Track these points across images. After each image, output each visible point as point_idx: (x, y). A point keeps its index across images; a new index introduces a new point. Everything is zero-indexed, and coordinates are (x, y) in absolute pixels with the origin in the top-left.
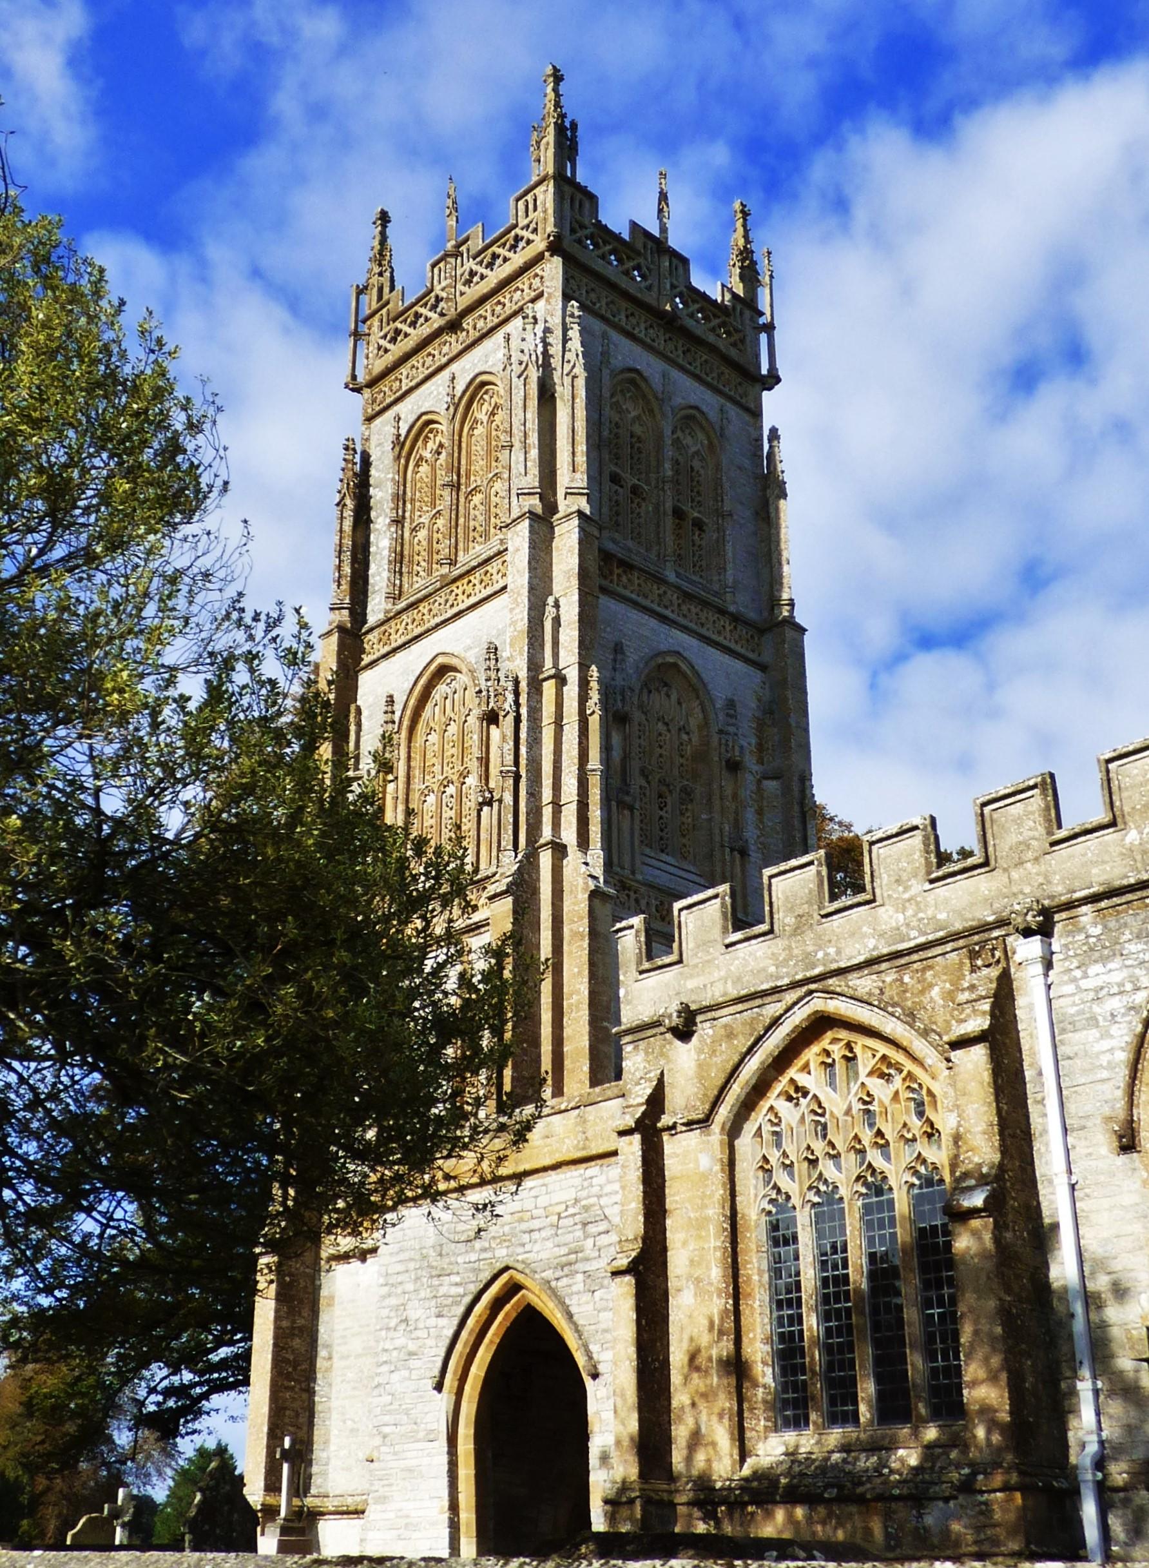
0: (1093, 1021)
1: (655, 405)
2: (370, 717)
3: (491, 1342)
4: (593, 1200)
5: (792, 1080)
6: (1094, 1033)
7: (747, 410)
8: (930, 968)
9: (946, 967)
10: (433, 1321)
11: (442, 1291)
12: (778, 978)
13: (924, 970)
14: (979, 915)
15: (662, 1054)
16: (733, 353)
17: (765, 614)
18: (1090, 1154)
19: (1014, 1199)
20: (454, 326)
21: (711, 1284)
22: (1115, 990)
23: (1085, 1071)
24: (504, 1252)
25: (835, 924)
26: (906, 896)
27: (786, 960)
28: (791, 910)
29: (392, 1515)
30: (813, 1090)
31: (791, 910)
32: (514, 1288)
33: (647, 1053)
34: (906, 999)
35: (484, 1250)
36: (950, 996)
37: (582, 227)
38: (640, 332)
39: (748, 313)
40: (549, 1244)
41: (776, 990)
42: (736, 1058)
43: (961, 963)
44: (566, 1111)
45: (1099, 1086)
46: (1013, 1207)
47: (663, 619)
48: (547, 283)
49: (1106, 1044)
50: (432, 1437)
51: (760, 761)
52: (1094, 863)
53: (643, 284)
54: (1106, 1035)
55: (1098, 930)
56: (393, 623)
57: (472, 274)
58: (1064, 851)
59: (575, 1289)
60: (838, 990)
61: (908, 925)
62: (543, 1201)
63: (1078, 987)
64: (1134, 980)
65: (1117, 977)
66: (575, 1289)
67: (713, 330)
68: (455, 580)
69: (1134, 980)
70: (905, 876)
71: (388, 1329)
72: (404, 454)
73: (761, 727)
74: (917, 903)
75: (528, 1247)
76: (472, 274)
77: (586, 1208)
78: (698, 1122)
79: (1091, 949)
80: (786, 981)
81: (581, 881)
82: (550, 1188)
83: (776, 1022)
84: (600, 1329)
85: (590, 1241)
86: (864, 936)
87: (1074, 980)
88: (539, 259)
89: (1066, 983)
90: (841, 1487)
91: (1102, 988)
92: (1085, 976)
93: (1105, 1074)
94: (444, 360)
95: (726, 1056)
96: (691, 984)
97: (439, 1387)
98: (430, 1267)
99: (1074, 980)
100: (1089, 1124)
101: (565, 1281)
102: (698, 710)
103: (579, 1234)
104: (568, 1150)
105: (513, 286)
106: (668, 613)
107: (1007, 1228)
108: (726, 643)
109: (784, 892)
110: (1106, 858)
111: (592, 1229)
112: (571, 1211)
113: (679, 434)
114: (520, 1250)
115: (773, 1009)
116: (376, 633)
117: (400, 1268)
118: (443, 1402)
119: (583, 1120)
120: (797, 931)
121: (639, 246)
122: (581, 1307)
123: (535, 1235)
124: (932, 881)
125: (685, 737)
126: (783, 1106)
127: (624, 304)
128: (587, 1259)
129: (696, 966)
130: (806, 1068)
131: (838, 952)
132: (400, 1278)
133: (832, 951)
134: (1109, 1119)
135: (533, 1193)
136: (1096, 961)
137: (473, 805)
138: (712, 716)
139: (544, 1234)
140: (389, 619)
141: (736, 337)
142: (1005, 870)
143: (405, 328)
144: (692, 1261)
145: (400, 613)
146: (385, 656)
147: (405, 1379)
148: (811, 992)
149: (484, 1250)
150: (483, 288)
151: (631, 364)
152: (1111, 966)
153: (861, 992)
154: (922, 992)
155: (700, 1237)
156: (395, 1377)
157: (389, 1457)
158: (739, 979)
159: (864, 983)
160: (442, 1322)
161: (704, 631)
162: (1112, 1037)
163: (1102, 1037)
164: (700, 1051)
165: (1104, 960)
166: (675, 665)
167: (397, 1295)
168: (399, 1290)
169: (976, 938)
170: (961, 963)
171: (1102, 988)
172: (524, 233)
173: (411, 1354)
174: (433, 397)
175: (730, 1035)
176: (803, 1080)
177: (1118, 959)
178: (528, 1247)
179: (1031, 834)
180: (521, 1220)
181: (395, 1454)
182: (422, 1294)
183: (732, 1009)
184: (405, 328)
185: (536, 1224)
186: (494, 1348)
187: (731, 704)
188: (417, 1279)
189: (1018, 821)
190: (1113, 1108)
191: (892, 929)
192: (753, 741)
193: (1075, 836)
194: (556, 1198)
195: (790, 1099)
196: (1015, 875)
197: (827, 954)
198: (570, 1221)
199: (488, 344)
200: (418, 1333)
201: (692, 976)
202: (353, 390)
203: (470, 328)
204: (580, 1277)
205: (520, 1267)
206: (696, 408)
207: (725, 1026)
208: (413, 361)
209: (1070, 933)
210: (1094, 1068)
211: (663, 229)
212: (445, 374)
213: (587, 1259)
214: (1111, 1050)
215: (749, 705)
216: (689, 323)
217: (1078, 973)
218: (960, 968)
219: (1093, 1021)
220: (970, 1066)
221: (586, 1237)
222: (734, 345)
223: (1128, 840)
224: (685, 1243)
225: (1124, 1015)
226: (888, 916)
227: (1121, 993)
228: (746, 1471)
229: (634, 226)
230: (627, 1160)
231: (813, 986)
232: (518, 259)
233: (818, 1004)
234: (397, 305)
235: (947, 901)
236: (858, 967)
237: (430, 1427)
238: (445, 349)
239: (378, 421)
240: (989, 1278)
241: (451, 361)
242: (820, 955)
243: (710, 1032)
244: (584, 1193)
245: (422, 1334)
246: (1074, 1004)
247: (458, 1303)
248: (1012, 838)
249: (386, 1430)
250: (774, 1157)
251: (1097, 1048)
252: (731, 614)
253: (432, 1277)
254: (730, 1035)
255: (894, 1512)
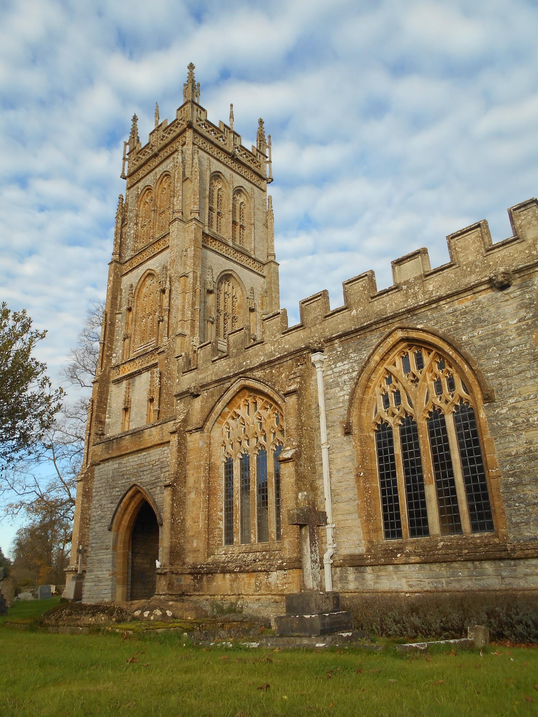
0: (338, 385)
1: (227, 184)
2: (125, 292)
3: (130, 512)
4: (165, 459)
5: (235, 412)
6: (338, 389)
7: (261, 189)
8: (282, 367)
9: (287, 366)
10: (110, 505)
11: (114, 493)
12: (230, 373)
13: (280, 368)
14: (299, 345)
15: (189, 403)
16: (256, 170)
17: (265, 259)
18: (335, 436)
19: (305, 455)
20: (156, 155)
21: (201, 490)
22: (346, 372)
23: (334, 405)
24: (134, 479)
25: (250, 352)
26: (275, 339)
27: (233, 366)
28: (236, 347)
29: (93, 577)
30: (242, 415)
31: (236, 347)
32: (138, 492)
33: (184, 403)
34: (273, 379)
35: (127, 478)
36: (287, 377)
37: (201, 120)
38: (222, 159)
39: (262, 156)
40: (149, 476)
41: (229, 378)
42: (214, 403)
43: (293, 364)
44: (157, 425)
45: (339, 410)
46: (305, 458)
47: (227, 258)
48: (187, 139)
49: (342, 393)
50: (107, 548)
51: (262, 309)
52: (340, 324)
53: (223, 143)
54: (342, 390)
55: (340, 349)
56: (133, 259)
57: (163, 136)
58: (330, 319)
59: (157, 492)
60: (249, 376)
61: (275, 351)
62: (148, 460)
63: (333, 371)
64: (352, 367)
65: (347, 367)
66: (157, 492)
67: (241, 155)
68: (154, 243)
69: (352, 367)
70: (275, 332)
71: (95, 508)
72: (139, 200)
73: (263, 297)
74: (279, 342)
75: (142, 477)
76: (163, 136)
77: (162, 462)
78: (199, 428)
79: (338, 356)
80: (232, 374)
81: (191, 348)
82: (151, 455)
83: (228, 389)
84: (163, 500)
85: (163, 474)
86: (260, 355)
87: (332, 369)
88: (184, 131)
89: (329, 370)
90: (241, 567)
91: (341, 371)
92: (336, 367)
93: (341, 405)
94: (153, 167)
95: (211, 402)
96: (200, 377)
97: (110, 529)
98: (110, 485)
99: (332, 369)
100: (335, 424)
101: (154, 489)
102: (240, 290)
103: (159, 472)
104: (157, 441)
105: (177, 140)
106: (229, 256)
107: (301, 465)
108: (251, 268)
109: (233, 340)
110: (344, 321)
111: (164, 470)
112: (157, 463)
113: (236, 196)
114: (140, 478)
115: (227, 385)
116: (128, 263)
117: (100, 485)
118: (111, 536)
119: (162, 429)
120: (237, 355)
121: (222, 129)
122: (158, 498)
123: (145, 473)
124: (283, 334)
125: (235, 300)
126: (230, 421)
127: (216, 149)
128: (161, 481)
129: (202, 369)
130: (239, 407)
131: (251, 362)
132: (101, 489)
133: (248, 362)
134: (342, 422)
135: (145, 457)
136: (340, 361)
137: (157, 322)
138: (245, 293)
139: (148, 472)
140: (132, 258)
141: (258, 164)
142: (309, 328)
143: (141, 156)
144: (195, 481)
145: (136, 255)
146: (131, 271)
147: (99, 526)
148: (241, 377)
149: (127, 478)
150: (166, 141)
151: (218, 170)
152: (345, 363)
153: (257, 377)
154: (279, 376)
155: (198, 472)
156: (97, 526)
157: (93, 555)
158: (217, 374)
159: (258, 374)
160: (113, 505)
161: (242, 263)
162: (344, 390)
163: (341, 391)
164: (202, 402)
165: (342, 361)
166: (231, 275)
167: (99, 496)
168: (100, 494)
169: (298, 354)
170: (293, 364)
171: (341, 371)
172: (180, 122)
173: (102, 517)
174: (149, 180)
175: (212, 395)
176: (238, 411)
177: (347, 360)
178: (142, 477)
179: (319, 313)
180: (140, 467)
181: (96, 554)
182: (107, 495)
183: (214, 385)
184: (141, 156)
185: (145, 468)
186: (131, 515)
187: (252, 289)
188: (106, 489)
189: (315, 309)
190: (343, 418)
191: (270, 352)
192: (260, 302)
193: (334, 313)
194: (153, 459)
195: (234, 419)
196: (313, 330)
197: (247, 363)
198: (157, 467)
199: (168, 161)
200: (105, 510)
201: (201, 374)
202: (123, 178)
203: (162, 156)
204: (159, 488)
205: (139, 484)
206: (242, 187)
207: (211, 392)
208: (143, 168)
209: (331, 351)
210: (338, 403)
211: (231, 125)
212: (154, 172)
213: (161, 481)
214: (344, 395)
215: (258, 291)
216: (240, 158)
217: (333, 366)
218: (292, 367)
219: (338, 385)
220: (291, 403)
221: (162, 473)
222: (257, 167)
223: (352, 314)
224: (193, 474)
225: (348, 382)
226: (269, 348)
227: (348, 373)
228: (210, 560)
229: (221, 122)
230: (173, 444)
231: (241, 375)
232: (178, 131)
233: (243, 382)
234: (138, 148)
235: (289, 341)
236: (257, 367)
237: (107, 544)
238: (154, 163)
239: (132, 189)
240: (292, 485)
241: (156, 167)
242: (245, 363)
243: (206, 394)
244: (161, 457)
245: (105, 510)
246: (331, 378)
247: (117, 498)
248: (312, 316)
249: (93, 545)
250: (261, 439)
251: (339, 394)
252: (253, 258)
253: (110, 489)
254: (212, 395)
255: (259, 577)
